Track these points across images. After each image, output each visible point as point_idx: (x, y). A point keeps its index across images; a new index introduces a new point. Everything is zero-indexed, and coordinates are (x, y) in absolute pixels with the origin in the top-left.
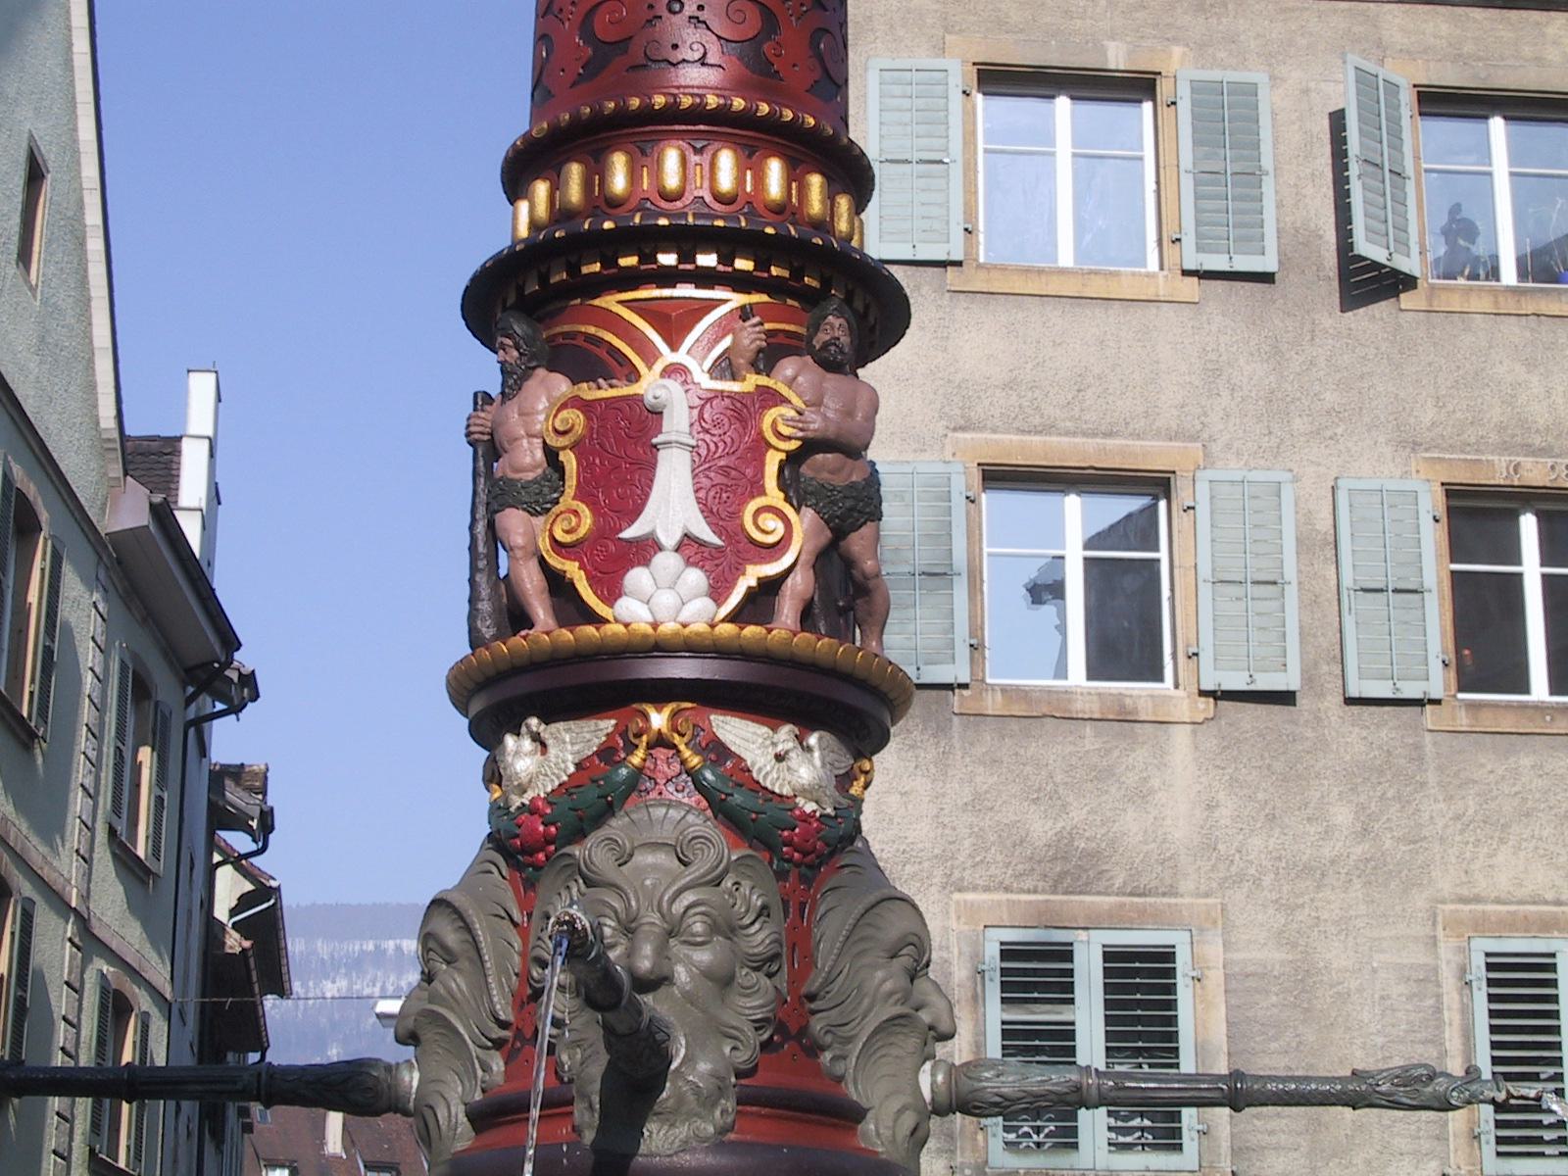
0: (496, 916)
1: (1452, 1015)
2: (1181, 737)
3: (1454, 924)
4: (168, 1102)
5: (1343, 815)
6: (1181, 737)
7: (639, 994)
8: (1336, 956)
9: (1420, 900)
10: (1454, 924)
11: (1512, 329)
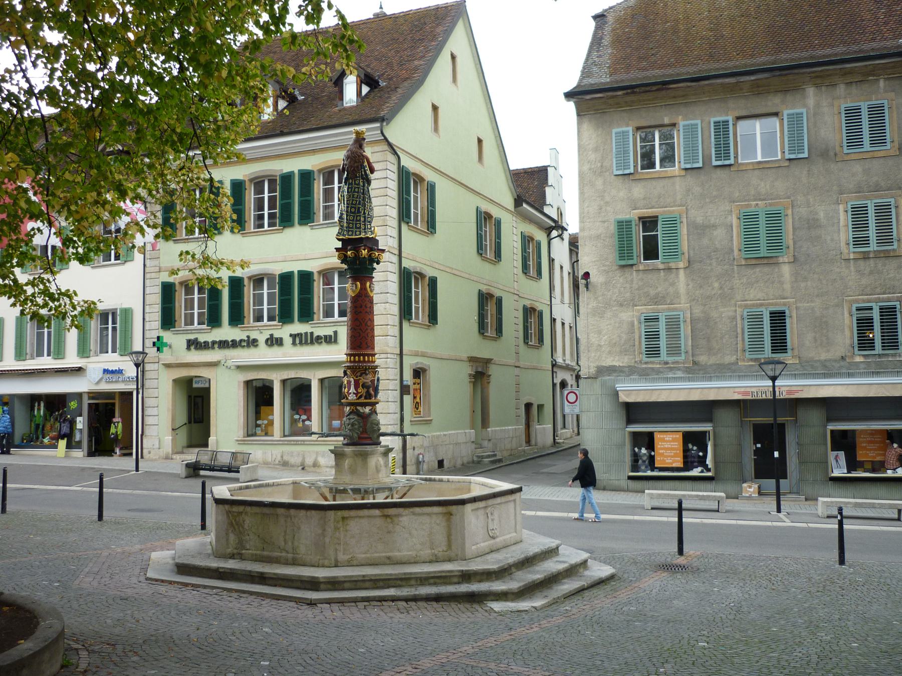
0: (405, 494)
1: (739, 326)
2: (682, 272)
3: (740, 306)
4: (383, 430)
5: (716, 285)
6: (682, 272)
7: (58, 91)
8: (714, 314)
9: (733, 302)
10: (740, 306)
11: (757, 172)
